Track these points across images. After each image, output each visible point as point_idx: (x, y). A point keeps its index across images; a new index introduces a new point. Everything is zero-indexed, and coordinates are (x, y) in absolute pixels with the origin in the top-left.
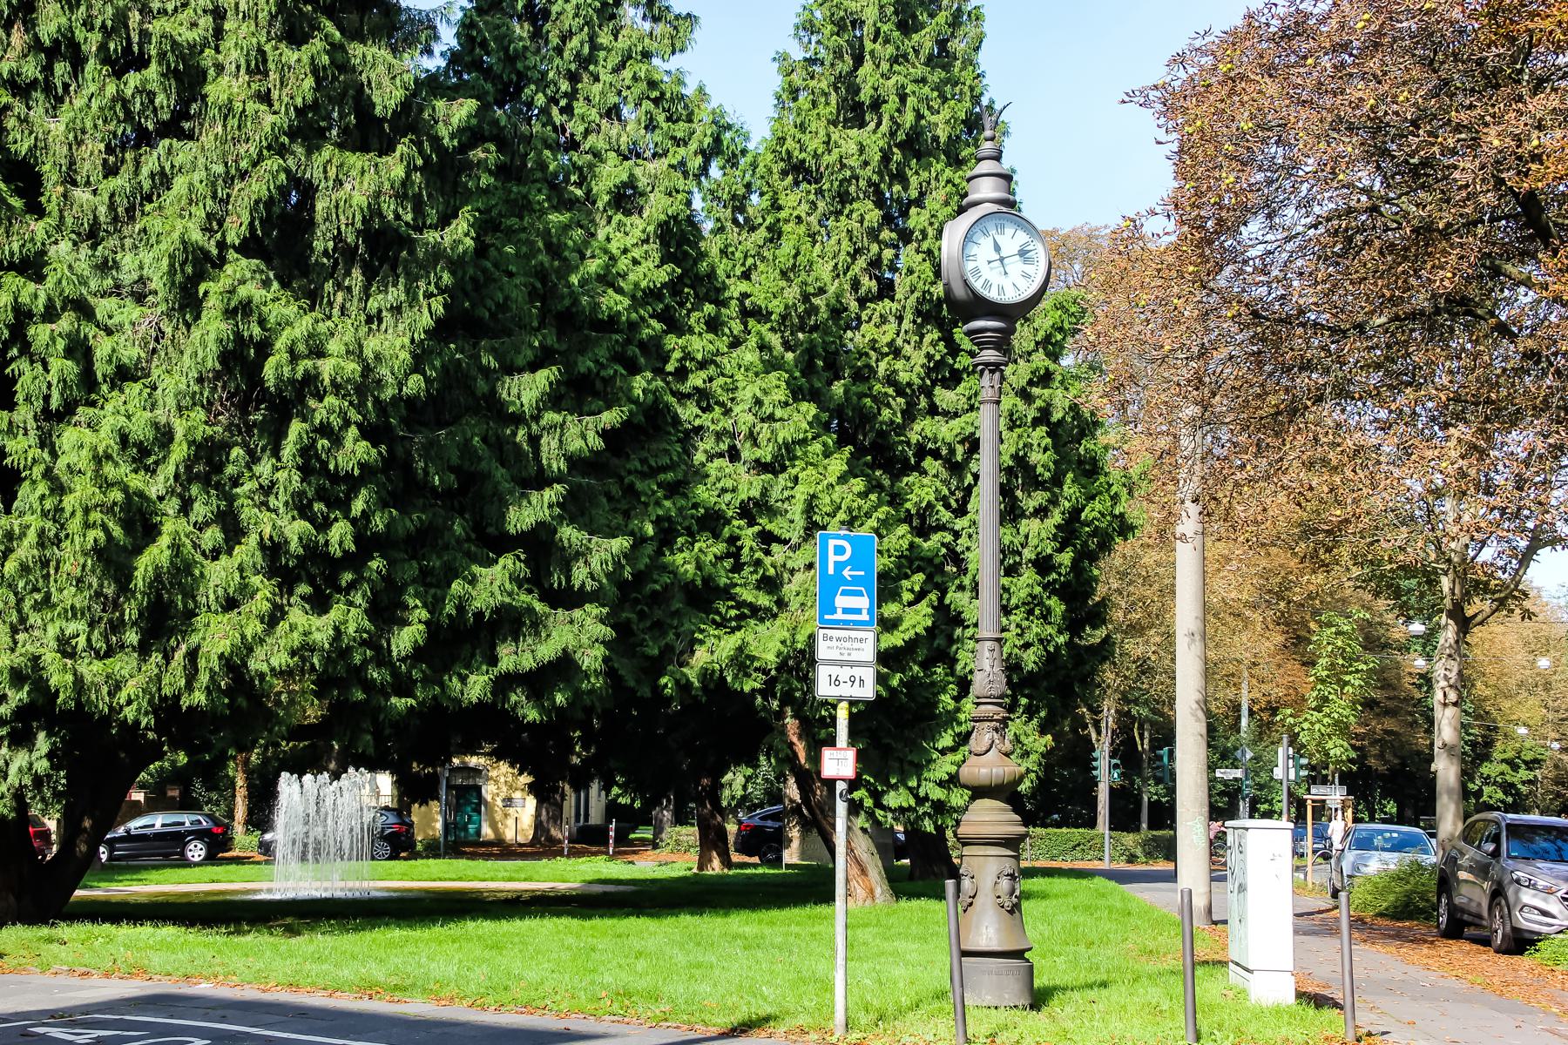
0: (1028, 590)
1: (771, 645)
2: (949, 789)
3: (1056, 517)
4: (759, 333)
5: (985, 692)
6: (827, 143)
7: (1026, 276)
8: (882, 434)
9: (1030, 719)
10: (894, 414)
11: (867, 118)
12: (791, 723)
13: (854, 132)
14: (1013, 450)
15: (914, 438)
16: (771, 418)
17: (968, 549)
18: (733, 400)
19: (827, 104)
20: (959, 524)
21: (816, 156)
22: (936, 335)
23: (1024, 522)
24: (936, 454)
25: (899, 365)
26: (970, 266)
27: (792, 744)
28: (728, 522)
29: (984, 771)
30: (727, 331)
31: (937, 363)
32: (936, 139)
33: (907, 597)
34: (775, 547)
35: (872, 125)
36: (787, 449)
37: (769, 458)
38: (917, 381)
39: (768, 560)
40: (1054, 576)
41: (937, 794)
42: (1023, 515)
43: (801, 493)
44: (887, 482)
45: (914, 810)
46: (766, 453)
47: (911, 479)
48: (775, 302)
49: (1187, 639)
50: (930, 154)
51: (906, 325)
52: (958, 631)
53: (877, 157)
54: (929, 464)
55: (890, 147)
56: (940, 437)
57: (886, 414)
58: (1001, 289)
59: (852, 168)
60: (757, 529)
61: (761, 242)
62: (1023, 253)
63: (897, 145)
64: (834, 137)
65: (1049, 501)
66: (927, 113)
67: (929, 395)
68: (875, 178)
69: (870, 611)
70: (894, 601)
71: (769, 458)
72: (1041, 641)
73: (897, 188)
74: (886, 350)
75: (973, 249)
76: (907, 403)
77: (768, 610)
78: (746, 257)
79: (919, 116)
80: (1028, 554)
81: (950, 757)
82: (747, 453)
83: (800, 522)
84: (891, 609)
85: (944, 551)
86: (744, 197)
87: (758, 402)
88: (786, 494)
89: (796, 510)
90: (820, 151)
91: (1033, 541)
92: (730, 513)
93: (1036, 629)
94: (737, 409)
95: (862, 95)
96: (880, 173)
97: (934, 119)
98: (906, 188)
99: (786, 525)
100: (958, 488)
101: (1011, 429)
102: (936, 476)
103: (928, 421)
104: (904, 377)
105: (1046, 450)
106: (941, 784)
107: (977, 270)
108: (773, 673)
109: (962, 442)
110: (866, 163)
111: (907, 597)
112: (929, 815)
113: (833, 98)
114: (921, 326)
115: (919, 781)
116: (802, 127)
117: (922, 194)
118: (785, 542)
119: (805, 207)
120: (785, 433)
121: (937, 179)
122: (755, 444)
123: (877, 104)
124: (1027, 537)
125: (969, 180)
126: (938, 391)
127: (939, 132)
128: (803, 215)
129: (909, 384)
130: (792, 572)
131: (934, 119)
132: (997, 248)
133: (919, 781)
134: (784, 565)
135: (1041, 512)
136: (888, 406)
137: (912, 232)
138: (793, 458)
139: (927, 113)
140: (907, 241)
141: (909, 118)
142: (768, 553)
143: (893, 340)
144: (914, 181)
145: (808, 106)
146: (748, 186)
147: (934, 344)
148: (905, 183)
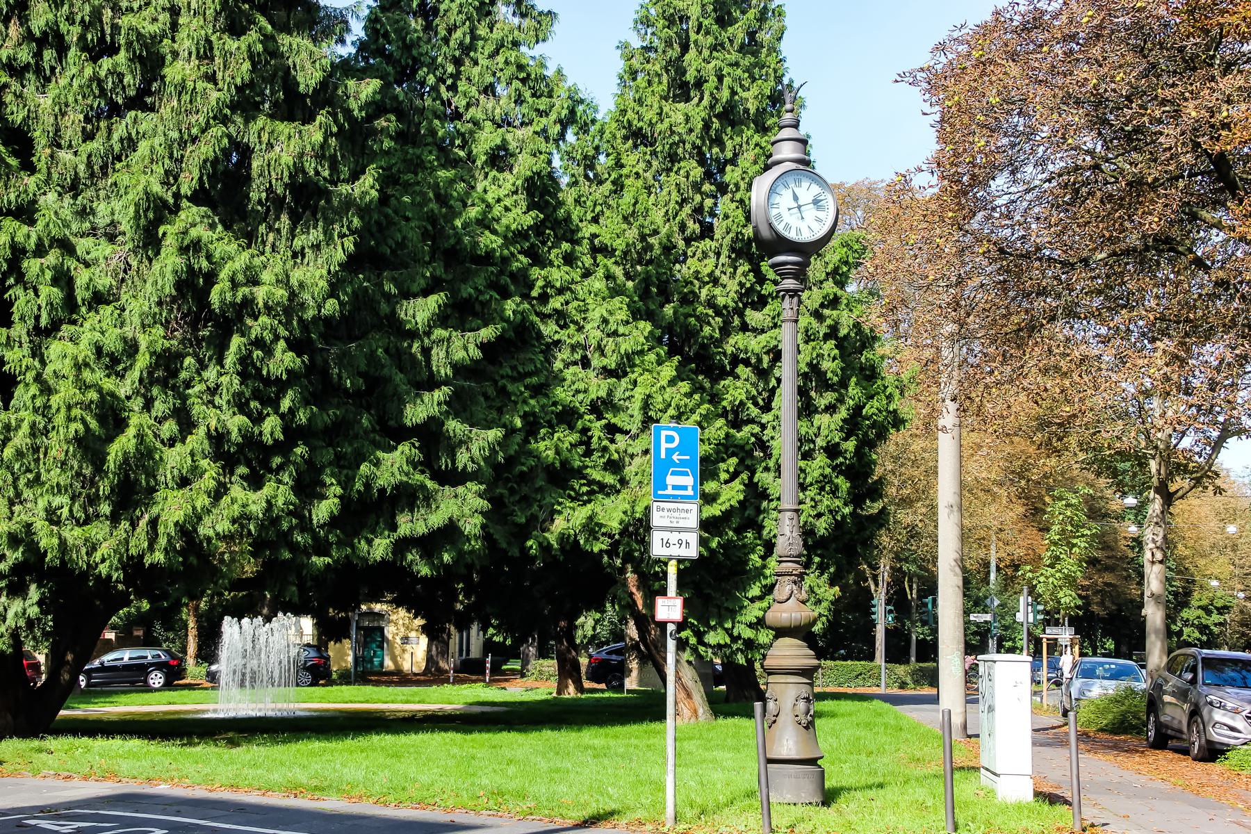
0: (820, 471)
1: (615, 515)
2: (757, 630)
3: (843, 413)
4: (605, 266)
5: (786, 552)
6: (660, 114)
7: (819, 220)
8: (704, 347)
9: (822, 574)
10: (714, 330)
11: (692, 94)
12: (631, 577)
13: (681, 106)
14: (808, 359)
15: (729, 349)
16: (615, 334)
17: (772, 438)
18: (584, 319)
19: (660, 83)
20: (765, 418)
21: (651, 124)
22: (747, 267)
23: (817, 416)
24: (747, 363)
25: (717, 291)
26: (774, 212)
27: (631, 594)
28: (581, 416)
29: (785, 615)
30: (580, 264)
31: (748, 290)
32: (747, 111)
33: (724, 476)
34: (618, 437)
35: (696, 100)
36: (628, 358)
37: (613, 366)
38: (732, 304)
39: (612, 447)
40: (841, 459)
41: (748, 633)
42: (816, 411)
43: (639, 393)
44: (707, 385)
45: (730, 646)
46: (611, 362)
47: (727, 382)
48: (619, 241)
49: (947, 510)
50: (742, 123)
51: (723, 259)
52: (765, 504)
53: (700, 125)
54: (741, 370)
55: (710, 117)
56: (750, 349)
57: (707, 330)
58: (799, 231)
59: (679, 134)
60: (604, 422)
61: (607, 194)
62: (816, 202)
63: (715, 116)
64: (666, 109)
65: (837, 400)
66: (739, 90)
67: (741, 315)
68: (698, 142)
69: (694, 488)
70: (713, 479)
71: (613, 366)
72: (831, 512)
73: (715, 150)
74: (707, 279)
75: (776, 199)
76: (724, 322)
77: (613, 486)
78: (595, 205)
79: (734, 93)
80: (820, 442)
81: (758, 604)
82: (596, 361)
83: (638, 417)
84: (711, 486)
85: (753, 439)
86: (594, 158)
87: (605, 321)
88: (627, 394)
89: (635, 407)
90: (654, 121)
91: (824, 432)
92: (582, 410)
93: (826, 502)
94: (588, 327)
95: (688, 76)
96: (702, 138)
97: (745, 95)
98: (723, 150)
99: (627, 419)
100: (764, 389)
101: (806, 342)
102: (746, 380)
103: (740, 336)
104: (721, 301)
105: (834, 359)
106: (751, 626)
107: (779, 216)
108: (617, 537)
109: (767, 353)
110: (691, 130)
111: (724, 476)
112: (741, 650)
113: (665, 79)
114: (735, 260)
115: (733, 623)
116: (640, 102)
117: (736, 155)
118: (627, 432)
119: (642, 165)
120: (626, 346)
121: (747, 143)
122: (603, 354)
123: (699, 83)
124: (819, 428)
125: (773, 144)
126: (748, 312)
127: (749, 105)
128: (641, 172)
129: (725, 307)
130: (632, 456)
131: (745, 95)
132: (796, 198)
133: (733, 623)
134: (626, 451)
135: (831, 409)
136: (709, 324)
137: (728, 185)
138: (633, 366)
139: (739, 90)
140: (724, 193)
141: (725, 94)
142: (612, 441)
143: (713, 272)
144: (729, 144)
145: (644, 84)
146: (597, 148)
147: (745, 274)
148: (722, 146)
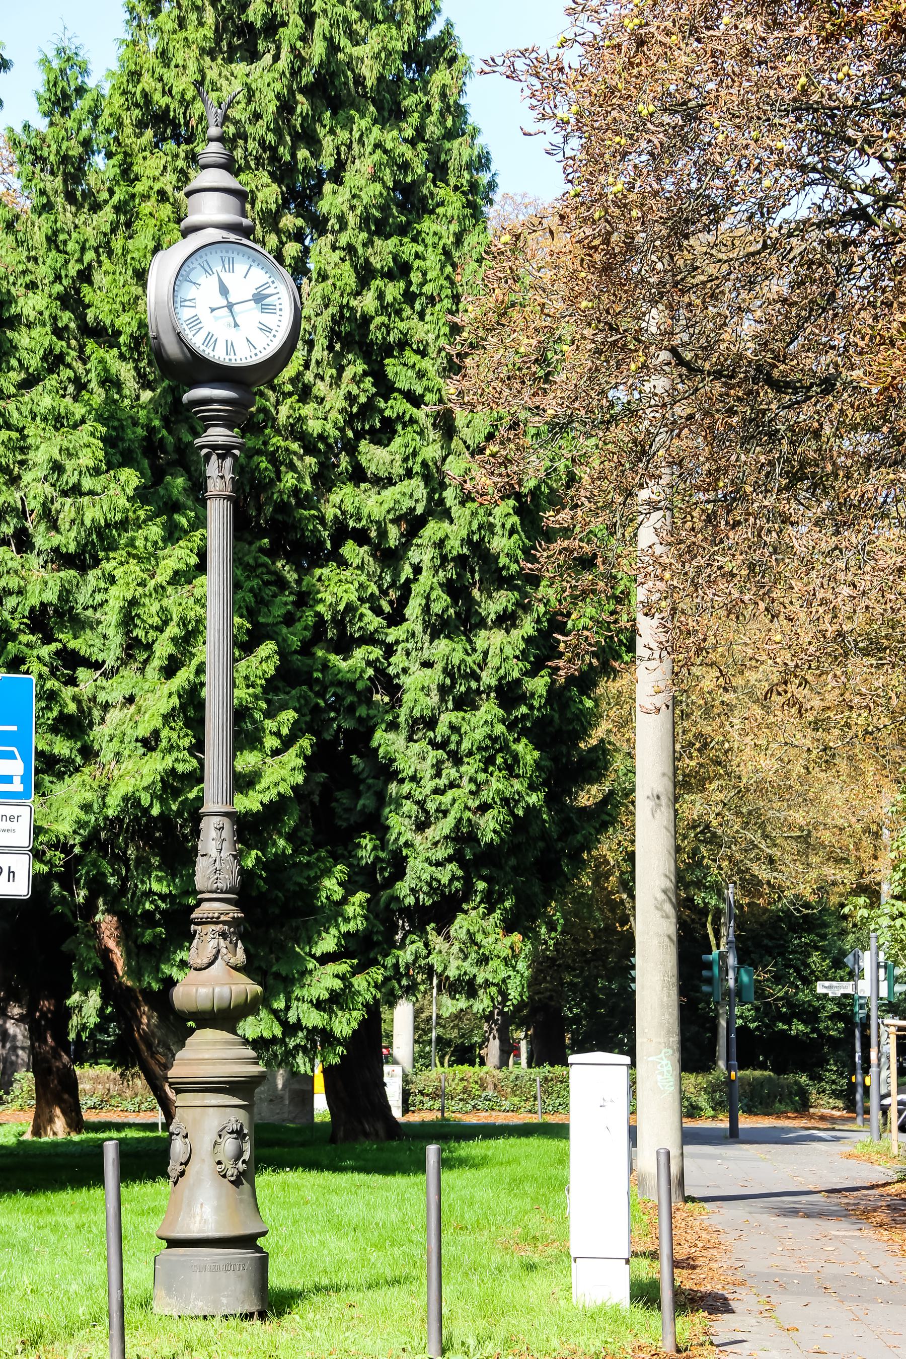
0: (487, 729)
1: (66, 811)
2: (331, 1012)
3: (528, 627)
4: (102, 361)
5: (210, 885)
6: (199, 84)
7: (265, 329)
8: (282, 507)
9: (491, 910)
10: (300, 479)
11: (260, 47)
12: (106, 922)
13: (240, 68)
14: (464, 533)
15: (330, 512)
16: (76, 490)
17: (405, 671)
18: (22, 463)
19: (201, 24)
20: (393, 634)
21: (186, 104)
22: (360, 367)
23: (483, 633)
24: (361, 537)
25: (308, 410)
26: (185, 314)
27: (108, 951)
28: (13, 636)
29: (203, 991)
30: (14, 363)
31: (363, 407)
32: (359, 81)
33: (271, 742)
34: (82, 673)
35: (268, 58)
36: (99, 535)
37: (72, 548)
38: (334, 433)
39: (67, 692)
40: (524, 709)
41: (313, 1019)
42: (482, 624)
43: (116, 597)
44: (291, 576)
45: (283, 1042)
46: (68, 541)
47: (325, 571)
48: (125, 318)
49: (650, 804)
50: (353, 105)
51: (319, 353)
52: (393, 788)
53: (272, 107)
54: (350, 549)
55: (291, 92)
56: (365, 512)
57: (289, 480)
58: (230, 347)
59: (236, 123)
60: (54, 646)
61: (107, 228)
62: (259, 298)
63: (302, 91)
64: (211, 75)
65: (518, 604)
66: (344, 42)
67: (351, 449)
68: (270, 138)
69: (24, 779)
70: (253, 749)
71: (72, 548)
72: (505, 801)
73: (303, 153)
74: (289, 388)
75: (188, 291)
76: (321, 464)
77: (70, 761)
78: (83, 250)
79: (333, 48)
80: (488, 678)
81: (333, 968)
82: (42, 539)
83: (116, 639)
84: (248, 760)
85: (370, 672)
86: (82, 160)
87: (57, 468)
88: (99, 597)
89: (111, 617)
90: (189, 96)
91: (494, 661)
92: (15, 625)
93: (496, 784)
94: (27, 477)
95: (250, 11)
96: (278, 131)
97: (357, 51)
98: (316, 154)
99: (98, 642)
100: (393, 585)
101: (463, 503)
102: (360, 567)
103: (348, 489)
104: (314, 427)
105: (512, 532)
106: (319, 1005)
107: (195, 321)
108: (77, 850)
109: (396, 521)
110: (257, 116)
111: (271, 742)
112: (305, 1050)
113: (210, 16)
114: (339, 356)
115: (288, 1000)
116: (164, 56)
117: (340, 165)
118: (97, 666)
119: (171, 178)
120: (93, 513)
121: (361, 141)
122: (54, 526)
123: (273, 25)
124: (486, 654)
125: (188, 194)
126: (364, 446)
127: (365, 71)
128: (169, 189)
129: (322, 437)
130: (106, 707)
131: (357, 51)
132: (224, 290)
133: (288, 1000)
134: (94, 699)
135: (507, 620)
136: (292, 467)
137: (326, 220)
138: (112, 546)
139: (344, 42)
140: (322, 232)
141: (317, 50)
142: (72, 681)
143: (299, 375)
144: (328, 144)
145: (170, 26)
146: (86, 143)
147: (357, 380)
148: (314, 144)
